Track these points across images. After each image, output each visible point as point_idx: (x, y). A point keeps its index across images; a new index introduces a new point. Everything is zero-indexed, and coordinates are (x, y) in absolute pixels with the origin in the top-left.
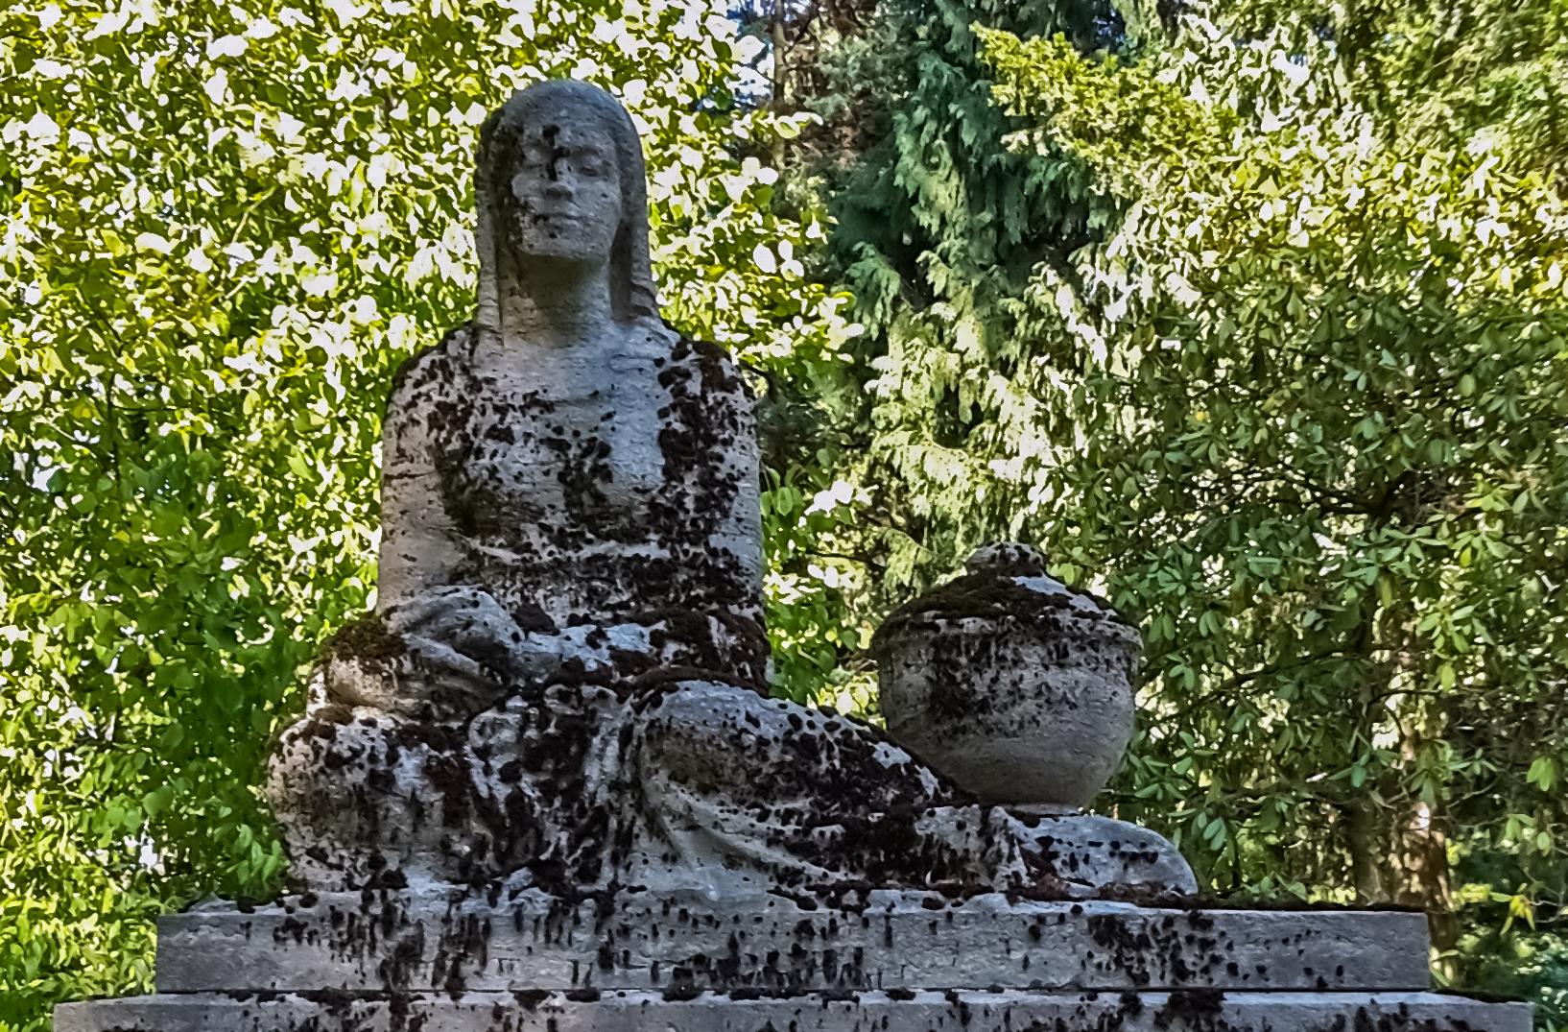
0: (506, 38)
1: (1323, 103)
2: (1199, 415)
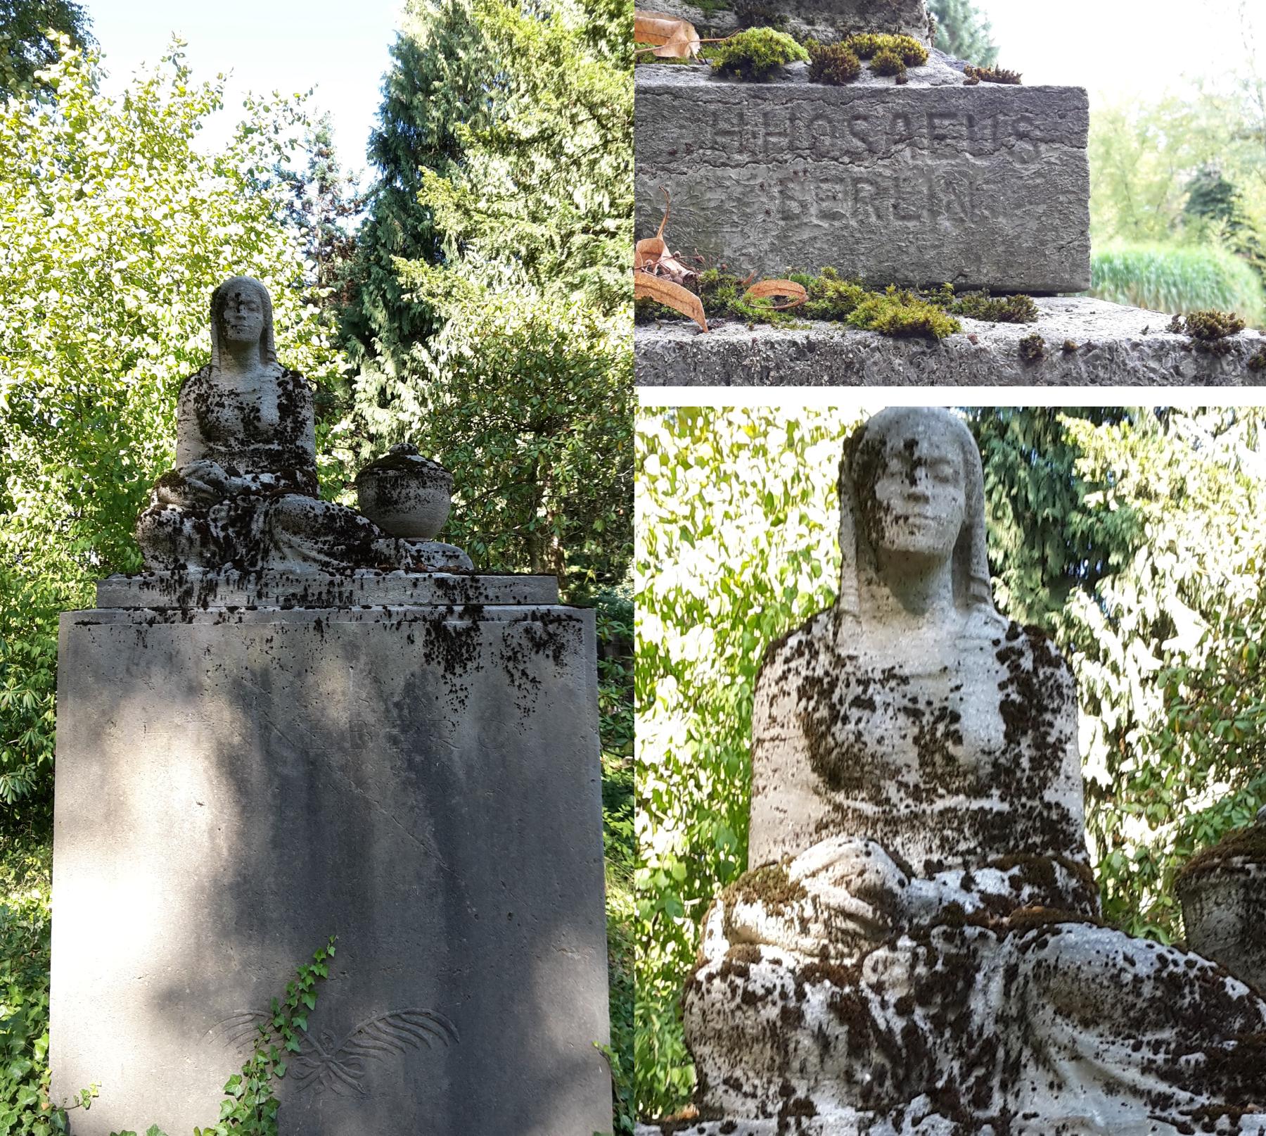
0: (221, 261)
1: (517, 283)
2: (473, 396)
